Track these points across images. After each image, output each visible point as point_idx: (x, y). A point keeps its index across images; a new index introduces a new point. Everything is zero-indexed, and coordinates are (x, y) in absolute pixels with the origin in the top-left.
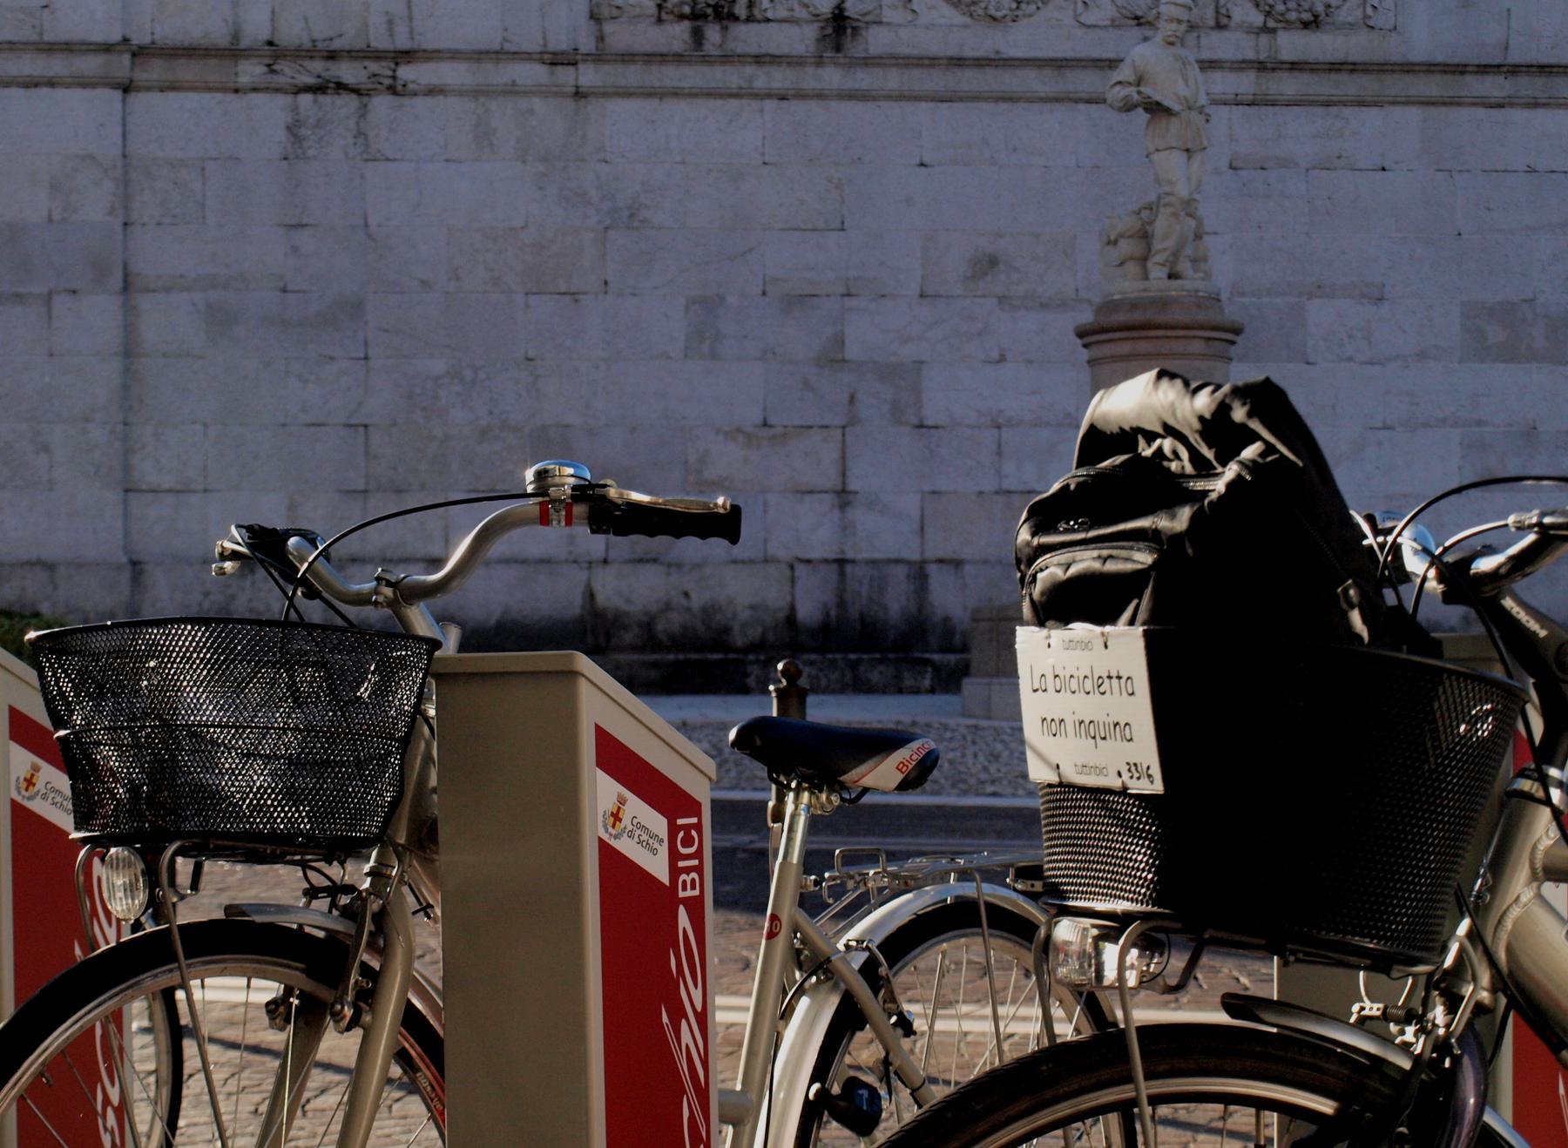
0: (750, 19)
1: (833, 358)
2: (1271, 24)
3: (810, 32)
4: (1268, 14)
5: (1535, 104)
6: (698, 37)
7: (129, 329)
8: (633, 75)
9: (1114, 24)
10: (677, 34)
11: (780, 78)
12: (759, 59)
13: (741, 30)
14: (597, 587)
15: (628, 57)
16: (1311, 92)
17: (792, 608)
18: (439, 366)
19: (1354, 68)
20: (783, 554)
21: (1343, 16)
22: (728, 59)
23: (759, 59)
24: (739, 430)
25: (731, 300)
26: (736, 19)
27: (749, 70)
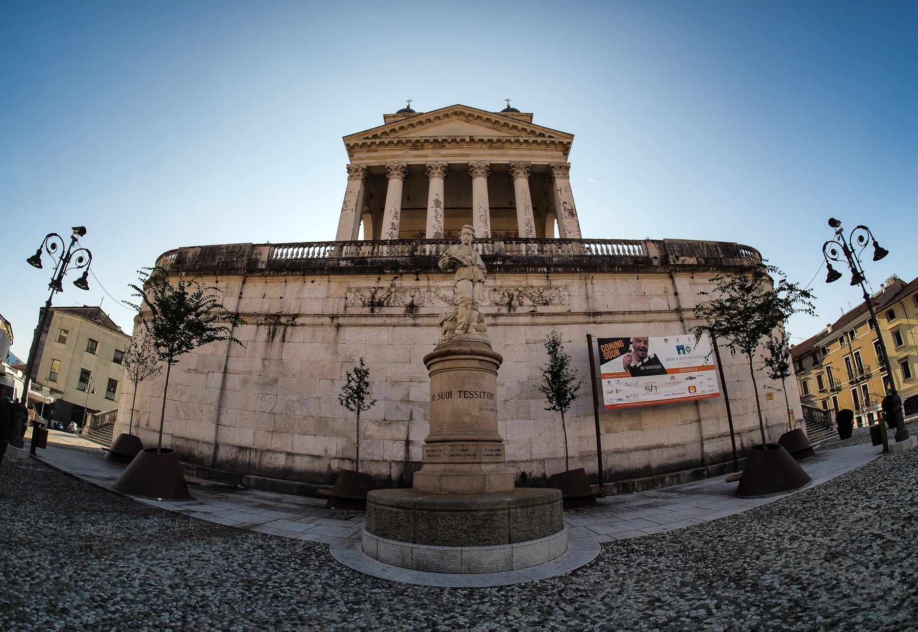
0: (388, 306)
1: (406, 400)
2: (535, 304)
3: (403, 309)
4: (534, 302)
5: (609, 323)
6: (372, 311)
7: (224, 382)
8: (353, 320)
9: (490, 305)
10: (367, 310)
11: (394, 320)
12: (388, 316)
13: (383, 308)
14: (332, 465)
15: (351, 316)
16: (641, 325)
17: (390, 475)
18: (295, 398)
19: (558, 314)
20: (388, 459)
21: (554, 302)
22: (382, 316)
23: (388, 316)
24: (377, 421)
25: (376, 382)
26: (384, 306)
27: (385, 318)
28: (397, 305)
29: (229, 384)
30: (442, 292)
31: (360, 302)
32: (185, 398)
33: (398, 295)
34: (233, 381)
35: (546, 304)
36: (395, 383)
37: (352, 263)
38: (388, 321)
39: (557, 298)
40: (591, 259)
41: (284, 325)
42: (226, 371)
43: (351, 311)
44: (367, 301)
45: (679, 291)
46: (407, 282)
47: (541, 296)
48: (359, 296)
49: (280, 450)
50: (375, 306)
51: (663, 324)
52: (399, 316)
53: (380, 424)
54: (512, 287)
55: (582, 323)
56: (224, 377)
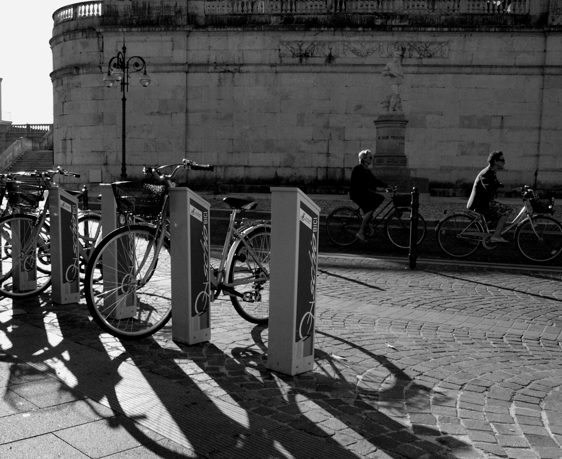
0: (312, 56)
1: (327, 126)
2: (421, 57)
3: (324, 59)
4: (421, 55)
5: (477, 74)
6: (301, 60)
7: (187, 120)
8: (288, 68)
10: (297, 60)
11: (318, 69)
12: (314, 65)
14: (278, 172)
15: (287, 65)
17: (317, 177)
20: (315, 166)
24: (307, 141)
27: (311, 67)
28: (318, 55)
29: (191, 121)
30: (353, 45)
31: (290, 53)
32: (152, 136)
33: (320, 47)
34: (194, 118)
35: (430, 57)
36: (320, 114)
37: (281, 19)
38: (314, 69)
39: (439, 52)
40: (473, 17)
41: (232, 72)
42: (187, 111)
43: (285, 60)
44: (296, 53)
45: (548, 49)
46: (325, 37)
47: (426, 50)
48: (290, 49)
49: (239, 165)
50: (302, 56)
51: (523, 77)
52: (321, 65)
53: (309, 143)
54: (405, 42)
55: (454, 73)
56: (187, 116)
